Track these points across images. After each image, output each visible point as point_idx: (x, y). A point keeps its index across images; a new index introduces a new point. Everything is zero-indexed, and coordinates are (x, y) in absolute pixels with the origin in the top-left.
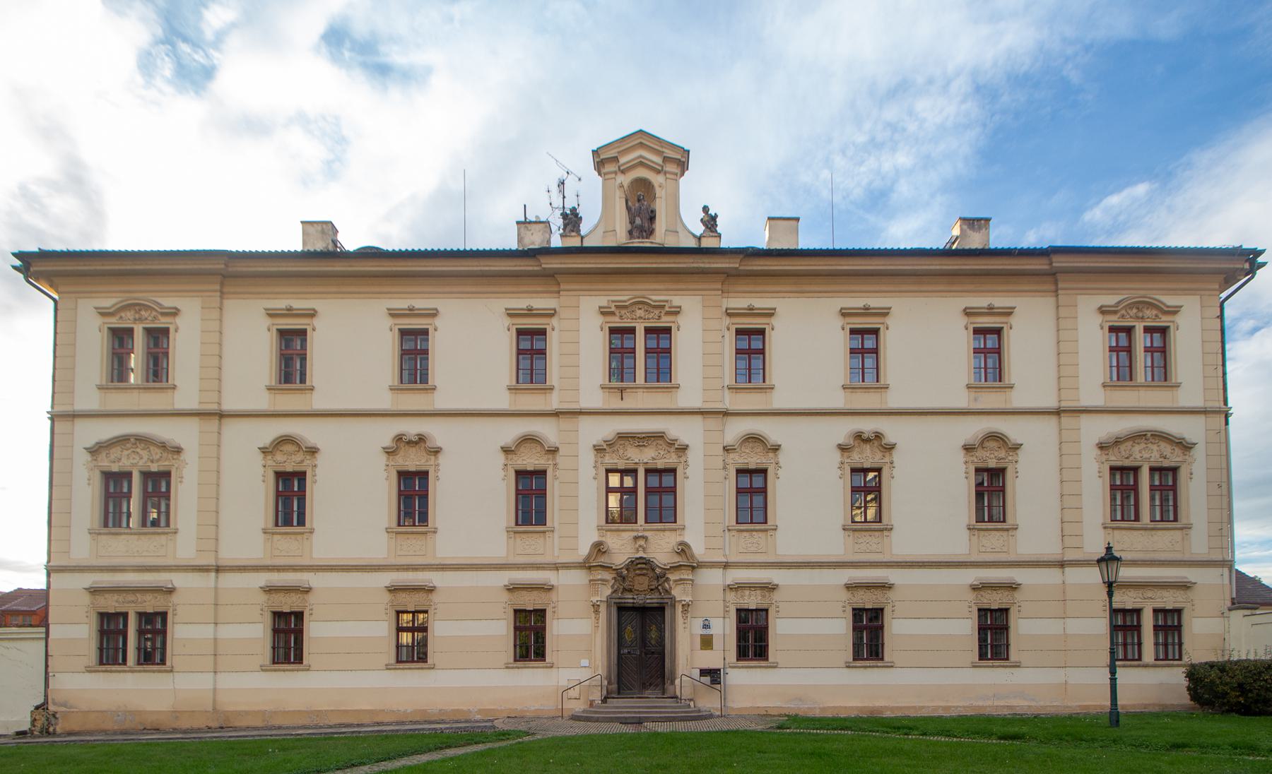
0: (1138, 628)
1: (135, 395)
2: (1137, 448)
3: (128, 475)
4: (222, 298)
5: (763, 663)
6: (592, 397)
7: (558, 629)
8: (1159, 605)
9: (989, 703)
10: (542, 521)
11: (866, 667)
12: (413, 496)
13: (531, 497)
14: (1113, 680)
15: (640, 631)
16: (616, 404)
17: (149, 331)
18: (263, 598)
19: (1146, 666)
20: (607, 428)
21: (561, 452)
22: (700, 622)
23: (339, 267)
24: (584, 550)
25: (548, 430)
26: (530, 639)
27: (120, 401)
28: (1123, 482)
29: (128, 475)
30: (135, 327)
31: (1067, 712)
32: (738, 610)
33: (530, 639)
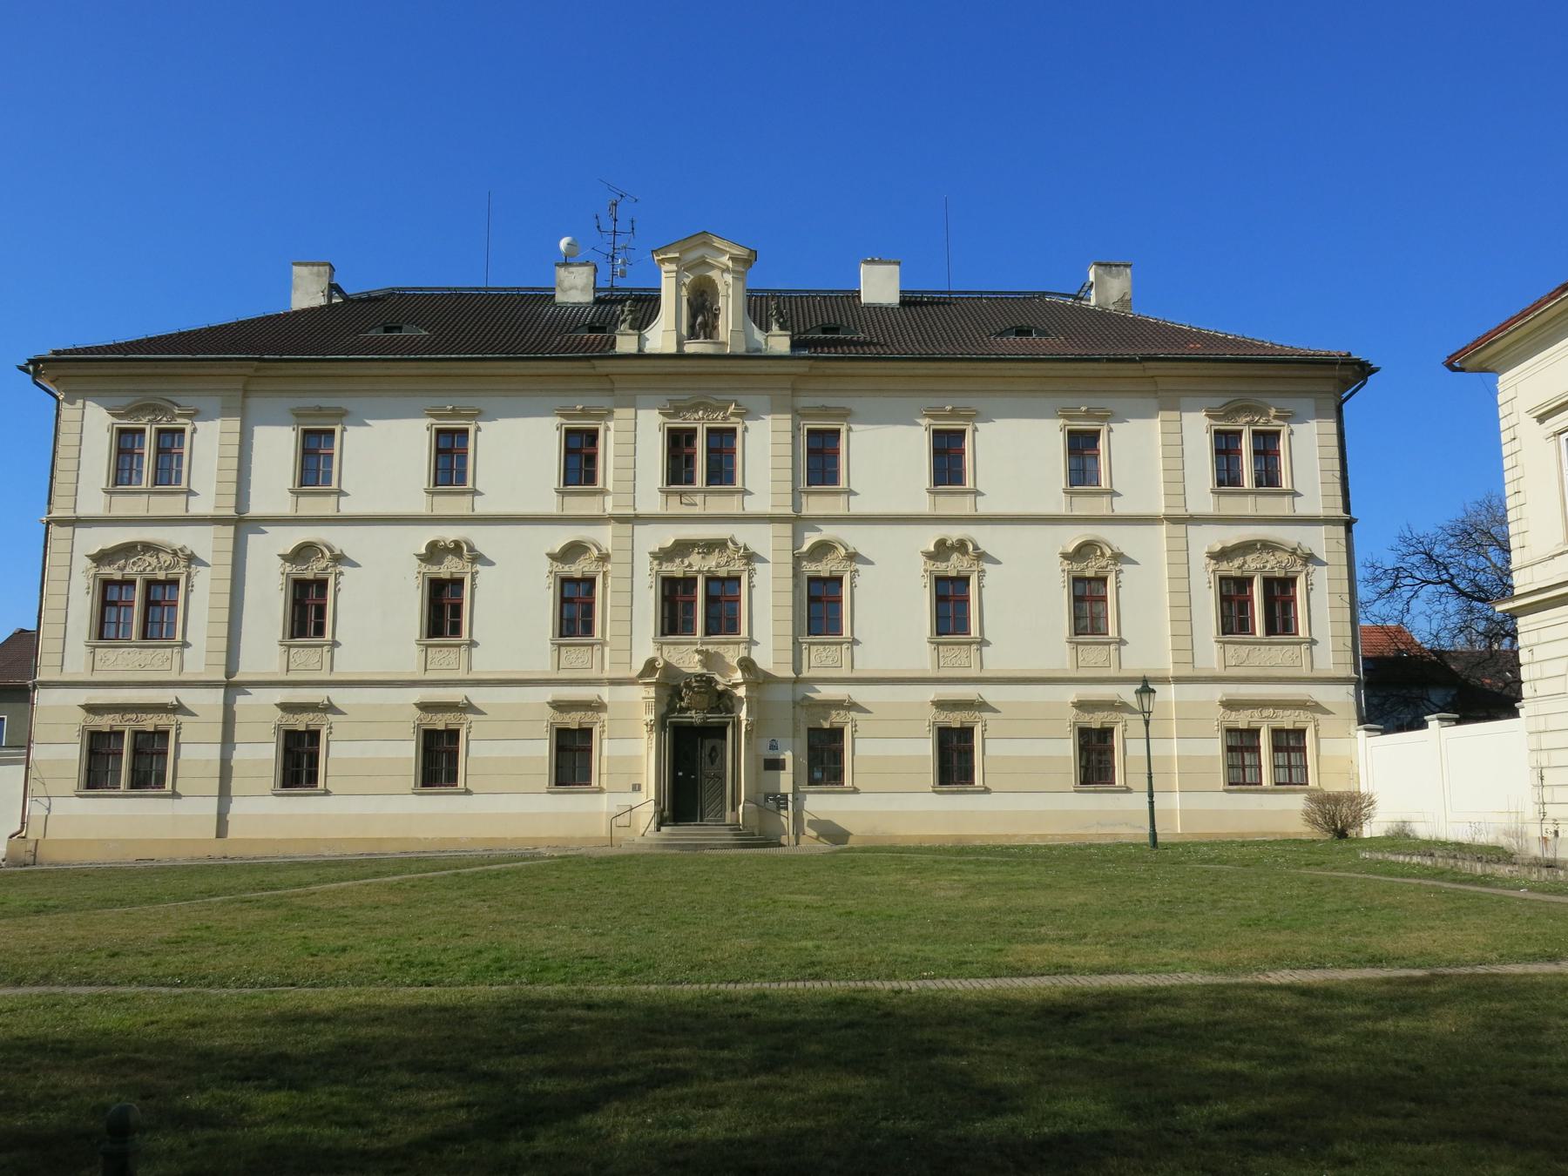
0: (1256, 749)
1: (1250, 499)
2: (1249, 558)
3: (132, 583)
4: (245, 397)
5: (838, 788)
6: (93, 501)
7: (605, 751)
8: (1277, 725)
9: (1093, 831)
10: (588, 629)
11: (953, 792)
12: (444, 610)
13: (576, 609)
14: (1151, 803)
15: (693, 747)
16: (675, 507)
17: (1256, 434)
18: (82, 713)
19: (1265, 791)
20: (667, 536)
21: (613, 559)
22: (766, 743)
23: (764, 367)
24: (639, 666)
25: (604, 536)
26: (572, 757)
27: (126, 505)
28: (1233, 595)
29: (132, 583)
30: (148, 428)
31: (129, 856)
32: (810, 730)
33: (572, 757)
